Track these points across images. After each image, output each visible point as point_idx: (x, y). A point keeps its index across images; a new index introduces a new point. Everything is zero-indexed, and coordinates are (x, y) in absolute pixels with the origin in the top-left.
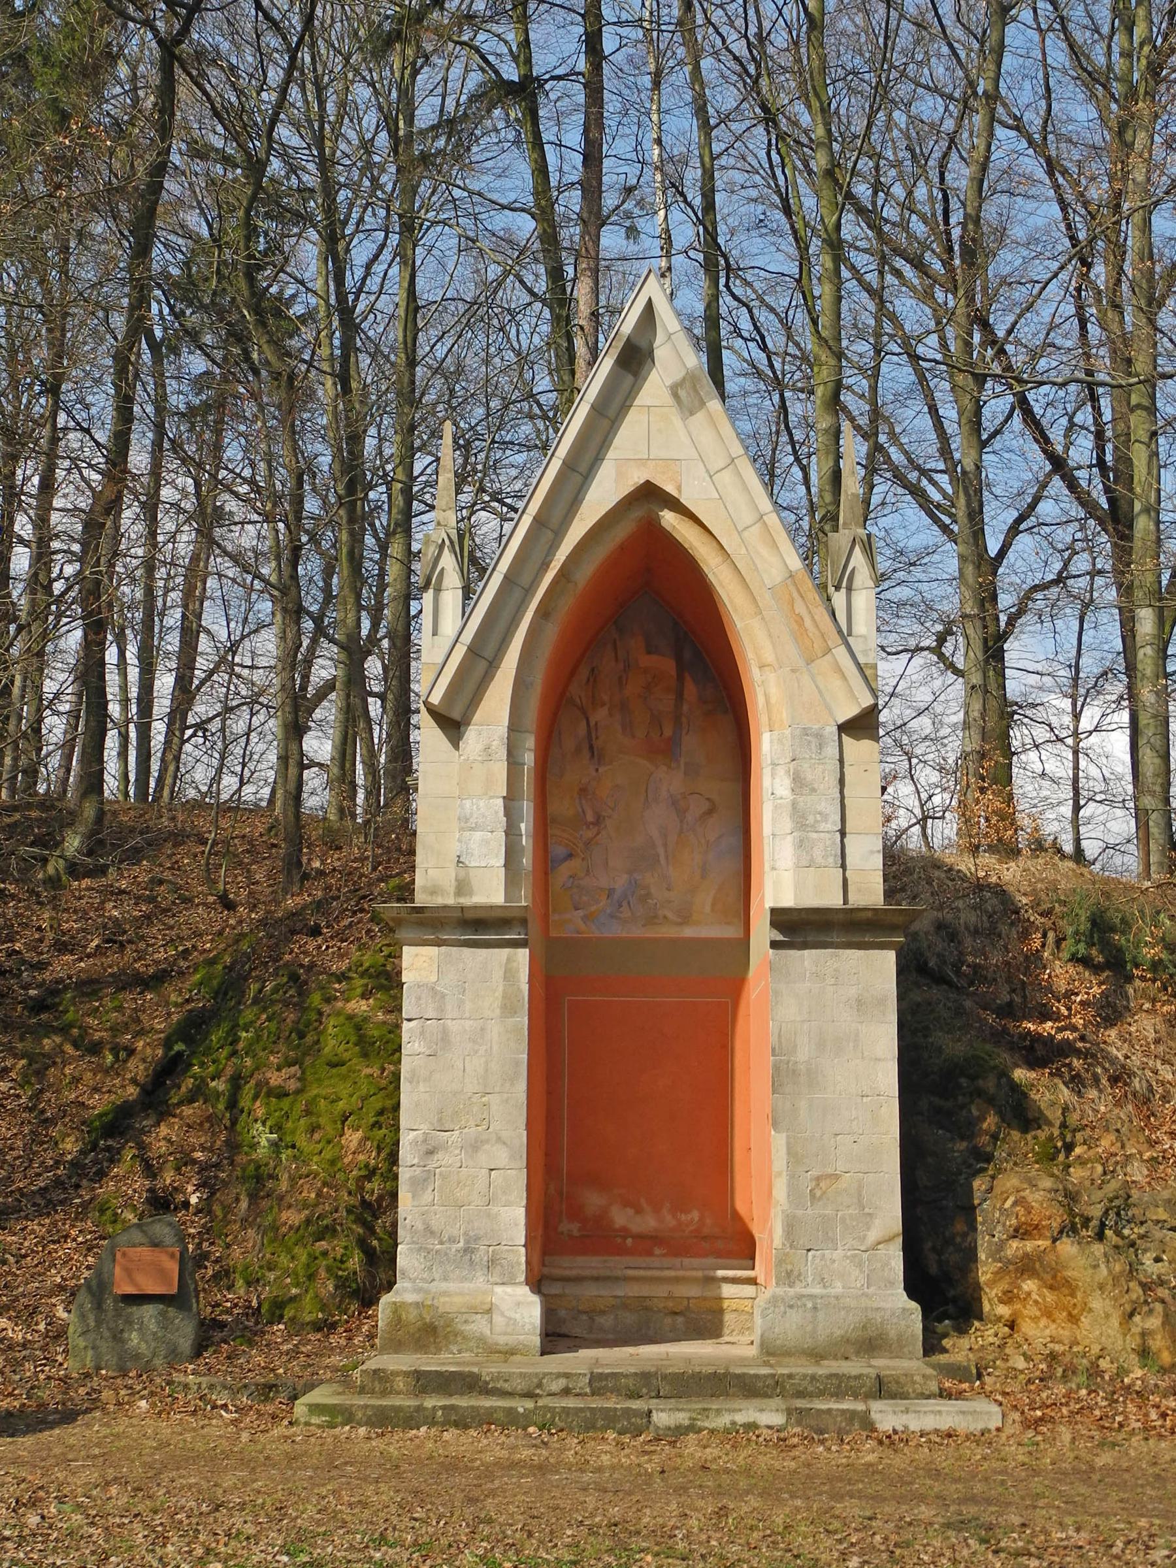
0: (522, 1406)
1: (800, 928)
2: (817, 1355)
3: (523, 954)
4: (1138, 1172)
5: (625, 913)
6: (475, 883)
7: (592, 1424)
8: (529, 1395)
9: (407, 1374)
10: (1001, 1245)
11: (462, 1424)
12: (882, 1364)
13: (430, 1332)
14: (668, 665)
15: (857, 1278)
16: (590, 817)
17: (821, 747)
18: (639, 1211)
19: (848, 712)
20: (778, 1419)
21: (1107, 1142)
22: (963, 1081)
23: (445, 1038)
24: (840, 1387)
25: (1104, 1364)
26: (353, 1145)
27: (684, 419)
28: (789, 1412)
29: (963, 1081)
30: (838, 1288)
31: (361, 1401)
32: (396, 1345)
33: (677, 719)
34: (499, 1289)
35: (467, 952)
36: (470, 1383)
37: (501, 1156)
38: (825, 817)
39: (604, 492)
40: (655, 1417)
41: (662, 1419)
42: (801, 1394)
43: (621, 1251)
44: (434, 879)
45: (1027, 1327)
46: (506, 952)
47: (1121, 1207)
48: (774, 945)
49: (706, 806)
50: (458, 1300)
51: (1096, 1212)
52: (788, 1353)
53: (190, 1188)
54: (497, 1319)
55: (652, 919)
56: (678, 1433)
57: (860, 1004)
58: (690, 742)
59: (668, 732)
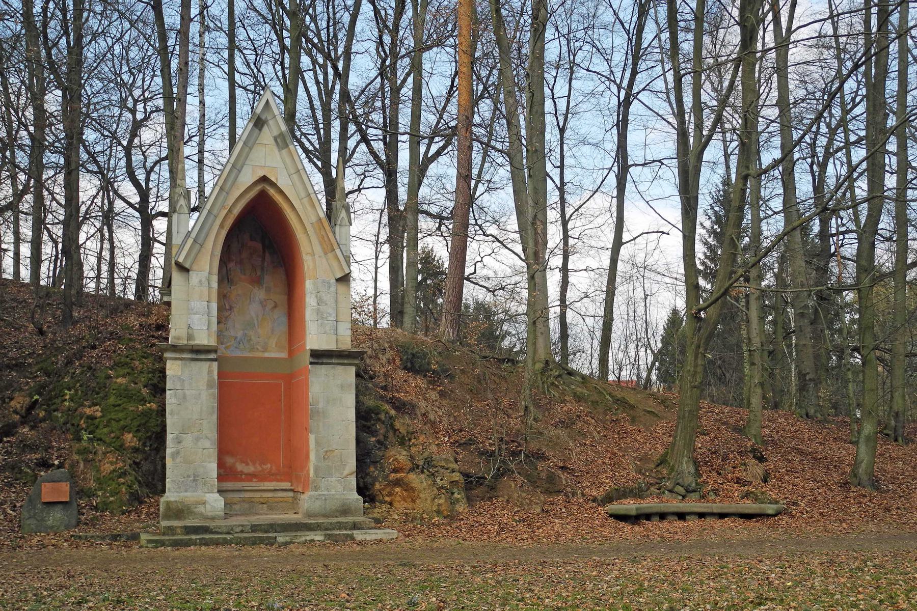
0: (228, 537)
1: (320, 357)
2: (325, 516)
3: (215, 364)
4: (434, 448)
5: (241, 346)
6: (196, 335)
7: (254, 542)
8: (228, 533)
9: (181, 527)
10: (388, 476)
11: (207, 544)
12: (350, 519)
13: (178, 512)
14: (259, 246)
15: (340, 488)
16: (227, 307)
17: (329, 287)
18: (247, 464)
19: (339, 275)
20: (321, 538)
21: (422, 438)
22: (373, 415)
23: (185, 397)
24: (341, 526)
25: (425, 516)
26: (129, 440)
27: (279, 151)
28: (325, 535)
29: (373, 415)
30: (333, 492)
31: (167, 538)
32: (167, 517)
33: (262, 269)
34: (207, 495)
35: (193, 363)
36: (205, 530)
37: (207, 444)
38: (330, 315)
39: (247, 178)
40: (278, 539)
41: (280, 539)
42: (327, 529)
43: (241, 480)
44: (177, 332)
45: (396, 504)
46: (209, 363)
47: (429, 462)
48: (311, 363)
49: (273, 304)
50: (192, 499)
51: (421, 463)
52: (316, 516)
53: (54, 458)
54: (207, 506)
55: (252, 349)
56: (286, 544)
57: (342, 387)
58: (267, 278)
59: (259, 273)
